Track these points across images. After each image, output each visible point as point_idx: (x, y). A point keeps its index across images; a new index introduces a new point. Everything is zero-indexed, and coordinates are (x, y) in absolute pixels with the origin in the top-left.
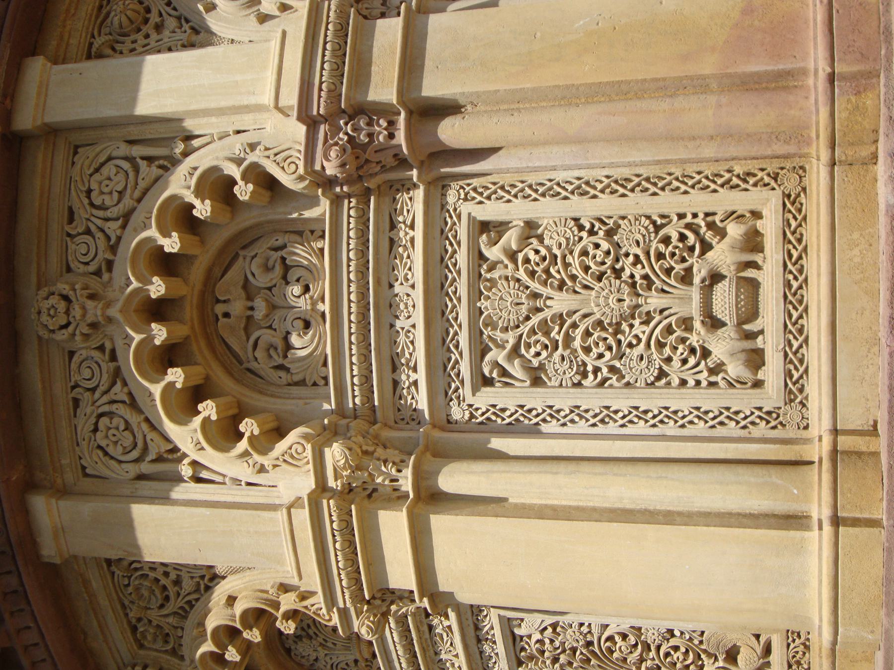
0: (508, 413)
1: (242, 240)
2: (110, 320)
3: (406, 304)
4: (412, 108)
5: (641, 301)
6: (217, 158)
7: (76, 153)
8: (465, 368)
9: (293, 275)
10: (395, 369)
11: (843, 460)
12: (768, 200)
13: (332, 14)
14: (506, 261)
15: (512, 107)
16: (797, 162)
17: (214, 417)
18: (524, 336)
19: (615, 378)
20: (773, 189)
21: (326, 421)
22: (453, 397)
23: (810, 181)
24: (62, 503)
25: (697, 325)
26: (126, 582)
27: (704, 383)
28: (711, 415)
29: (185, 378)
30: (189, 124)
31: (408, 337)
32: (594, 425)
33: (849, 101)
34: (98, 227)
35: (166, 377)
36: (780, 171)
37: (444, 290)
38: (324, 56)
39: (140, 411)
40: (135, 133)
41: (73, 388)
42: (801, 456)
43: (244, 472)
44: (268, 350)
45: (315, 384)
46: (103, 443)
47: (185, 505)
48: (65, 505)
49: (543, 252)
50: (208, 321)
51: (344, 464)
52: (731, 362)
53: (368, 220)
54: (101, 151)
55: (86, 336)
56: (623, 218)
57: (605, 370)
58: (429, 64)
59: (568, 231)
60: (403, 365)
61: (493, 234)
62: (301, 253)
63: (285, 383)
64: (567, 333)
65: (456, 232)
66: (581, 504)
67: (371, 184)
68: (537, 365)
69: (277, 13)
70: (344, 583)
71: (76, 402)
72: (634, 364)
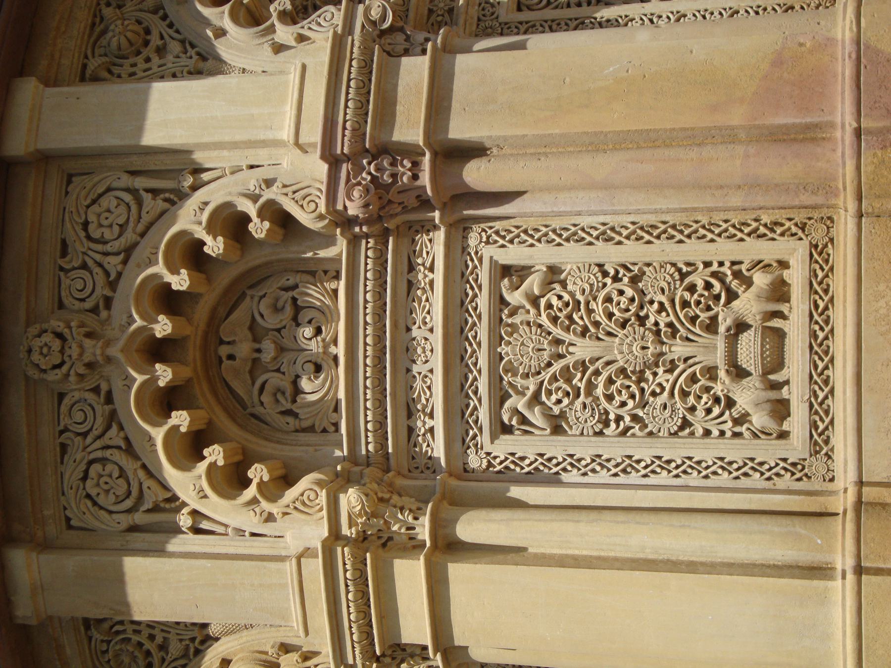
0: (527, 462)
1: (256, 274)
2: (109, 360)
3: (424, 348)
4: (437, 149)
5: (665, 349)
6: (230, 194)
7: (69, 182)
8: (483, 415)
9: (305, 316)
10: (410, 415)
11: (867, 510)
12: (795, 250)
13: (355, 50)
14: (528, 307)
15: (539, 151)
16: (825, 213)
17: (221, 463)
18: (546, 382)
19: (637, 427)
20: (801, 239)
21: (339, 468)
22: (471, 445)
23: (837, 232)
24: (43, 557)
25: (722, 374)
26: (105, 648)
27: (729, 434)
28: (735, 466)
29: (190, 421)
30: (199, 157)
31: (425, 382)
32: (616, 475)
33: (875, 155)
34: (96, 262)
35: (169, 420)
36: (807, 221)
37: (464, 335)
38: (347, 93)
39: (137, 457)
40: (137, 163)
41: (62, 432)
42: (826, 508)
43: (250, 521)
44: (275, 395)
45: (324, 431)
46: (93, 492)
47: (183, 557)
48: (49, 559)
49: (566, 297)
50: (211, 363)
51: (360, 510)
52: (756, 413)
53: (386, 261)
54: (100, 181)
55: (81, 377)
56: (648, 265)
57: (627, 419)
58: (455, 105)
59: (592, 277)
60: (419, 411)
61: (514, 278)
62: (314, 294)
63: (293, 429)
64: (589, 381)
65: (477, 275)
66: (602, 554)
67: (390, 225)
68: (557, 413)
69: (294, 44)
70: (355, 637)
71: (64, 447)
72: (657, 412)
